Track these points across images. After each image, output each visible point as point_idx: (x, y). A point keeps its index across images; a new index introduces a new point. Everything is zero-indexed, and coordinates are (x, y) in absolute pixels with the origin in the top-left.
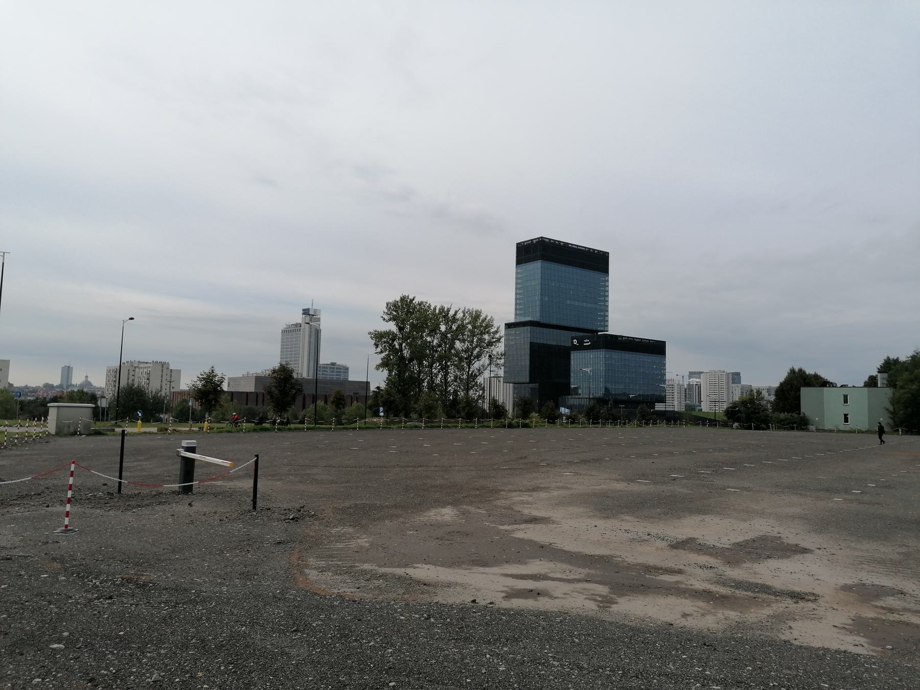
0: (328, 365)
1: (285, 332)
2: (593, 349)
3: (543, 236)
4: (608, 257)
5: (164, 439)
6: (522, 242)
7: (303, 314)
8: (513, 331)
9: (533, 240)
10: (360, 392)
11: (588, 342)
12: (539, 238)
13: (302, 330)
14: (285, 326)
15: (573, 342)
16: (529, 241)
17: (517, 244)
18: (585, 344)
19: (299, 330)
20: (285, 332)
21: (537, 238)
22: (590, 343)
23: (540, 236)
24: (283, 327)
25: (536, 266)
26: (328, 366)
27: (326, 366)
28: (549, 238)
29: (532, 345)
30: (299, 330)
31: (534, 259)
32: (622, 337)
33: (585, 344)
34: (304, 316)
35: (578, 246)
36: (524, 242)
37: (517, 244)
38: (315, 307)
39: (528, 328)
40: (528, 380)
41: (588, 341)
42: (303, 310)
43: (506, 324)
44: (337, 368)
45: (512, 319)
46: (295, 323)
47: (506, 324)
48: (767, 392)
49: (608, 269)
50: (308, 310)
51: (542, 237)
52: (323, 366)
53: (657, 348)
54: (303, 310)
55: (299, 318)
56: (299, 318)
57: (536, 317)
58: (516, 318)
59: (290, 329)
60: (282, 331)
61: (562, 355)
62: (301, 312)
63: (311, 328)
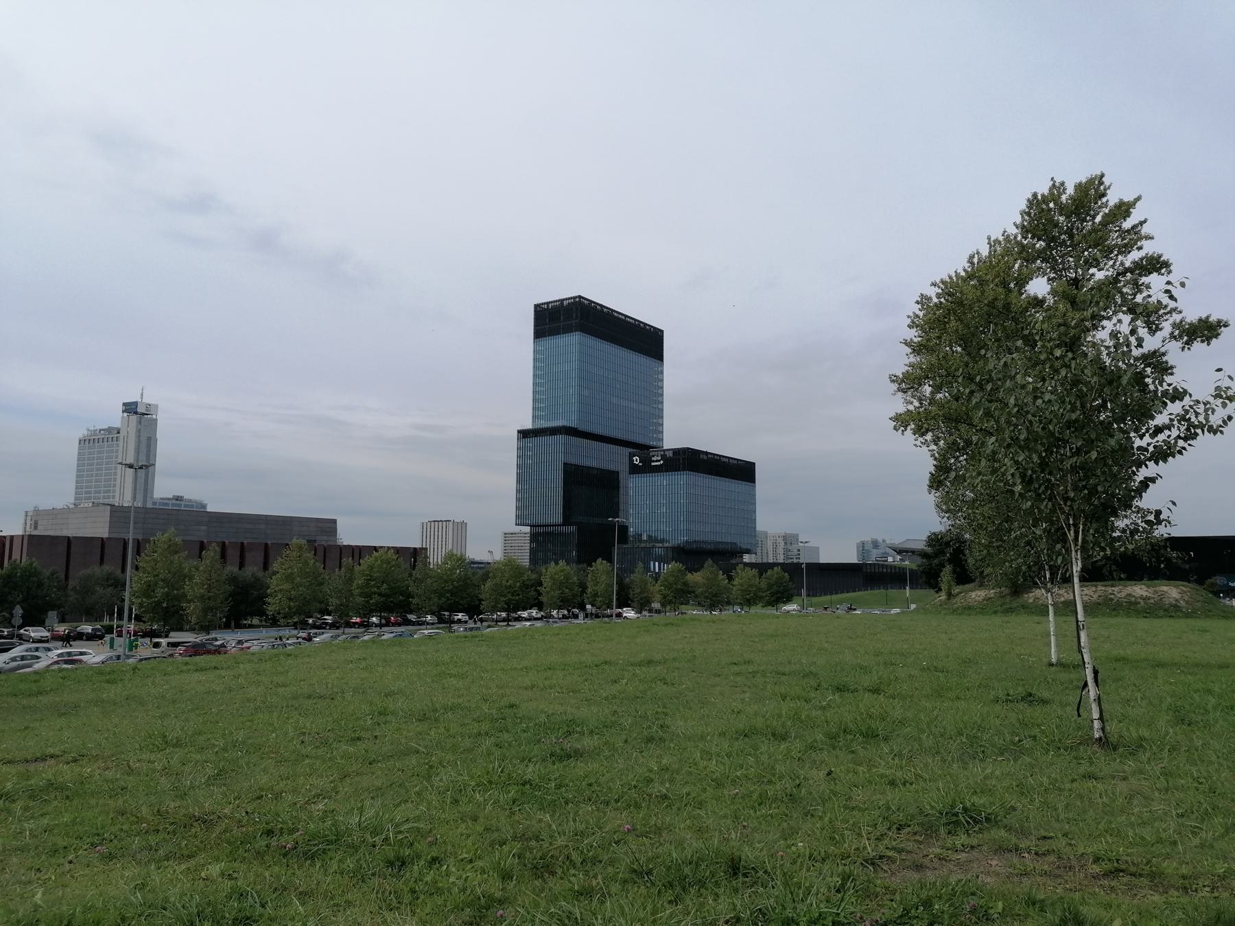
0: (169, 499)
1: (92, 442)
2: (667, 471)
3: (582, 295)
4: (663, 336)
5: (1135, 662)
6: (545, 303)
7: (123, 412)
8: (530, 442)
9: (564, 300)
10: (318, 538)
11: (659, 461)
12: (574, 298)
13: (122, 437)
14: (86, 433)
15: (631, 461)
16: (556, 301)
17: (536, 306)
18: (653, 464)
19: (101, 440)
20: (92, 442)
21: (571, 298)
22: (662, 462)
23: (577, 295)
24: (82, 433)
25: (571, 343)
26: (170, 502)
27: (166, 501)
28: (545, 301)
29: (565, 464)
30: (101, 440)
31: (567, 330)
32: (707, 453)
33: (653, 464)
34: (125, 414)
35: (626, 316)
36: (548, 303)
37: (536, 306)
38: (146, 400)
39: (560, 438)
40: (560, 520)
41: (659, 458)
42: (124, 404)
43: (519, 432)
44: (185, 506)
45: (528, 425)
46: (106, 427)
47: (519, 432)
48: (784, 540)
49: (663, 356)
50: (136, 403)
51: (580, 297)
52: (161, 501)
53: (743, 472)
54: (124, 404)
55: (115, 418)
56: (115, 418)
57: (572, 422)
58: (533, 422)
59: (97, 437)
60: (80, 441)
61: (607, 483)
62: (121, 408)
63: (139, 436)
